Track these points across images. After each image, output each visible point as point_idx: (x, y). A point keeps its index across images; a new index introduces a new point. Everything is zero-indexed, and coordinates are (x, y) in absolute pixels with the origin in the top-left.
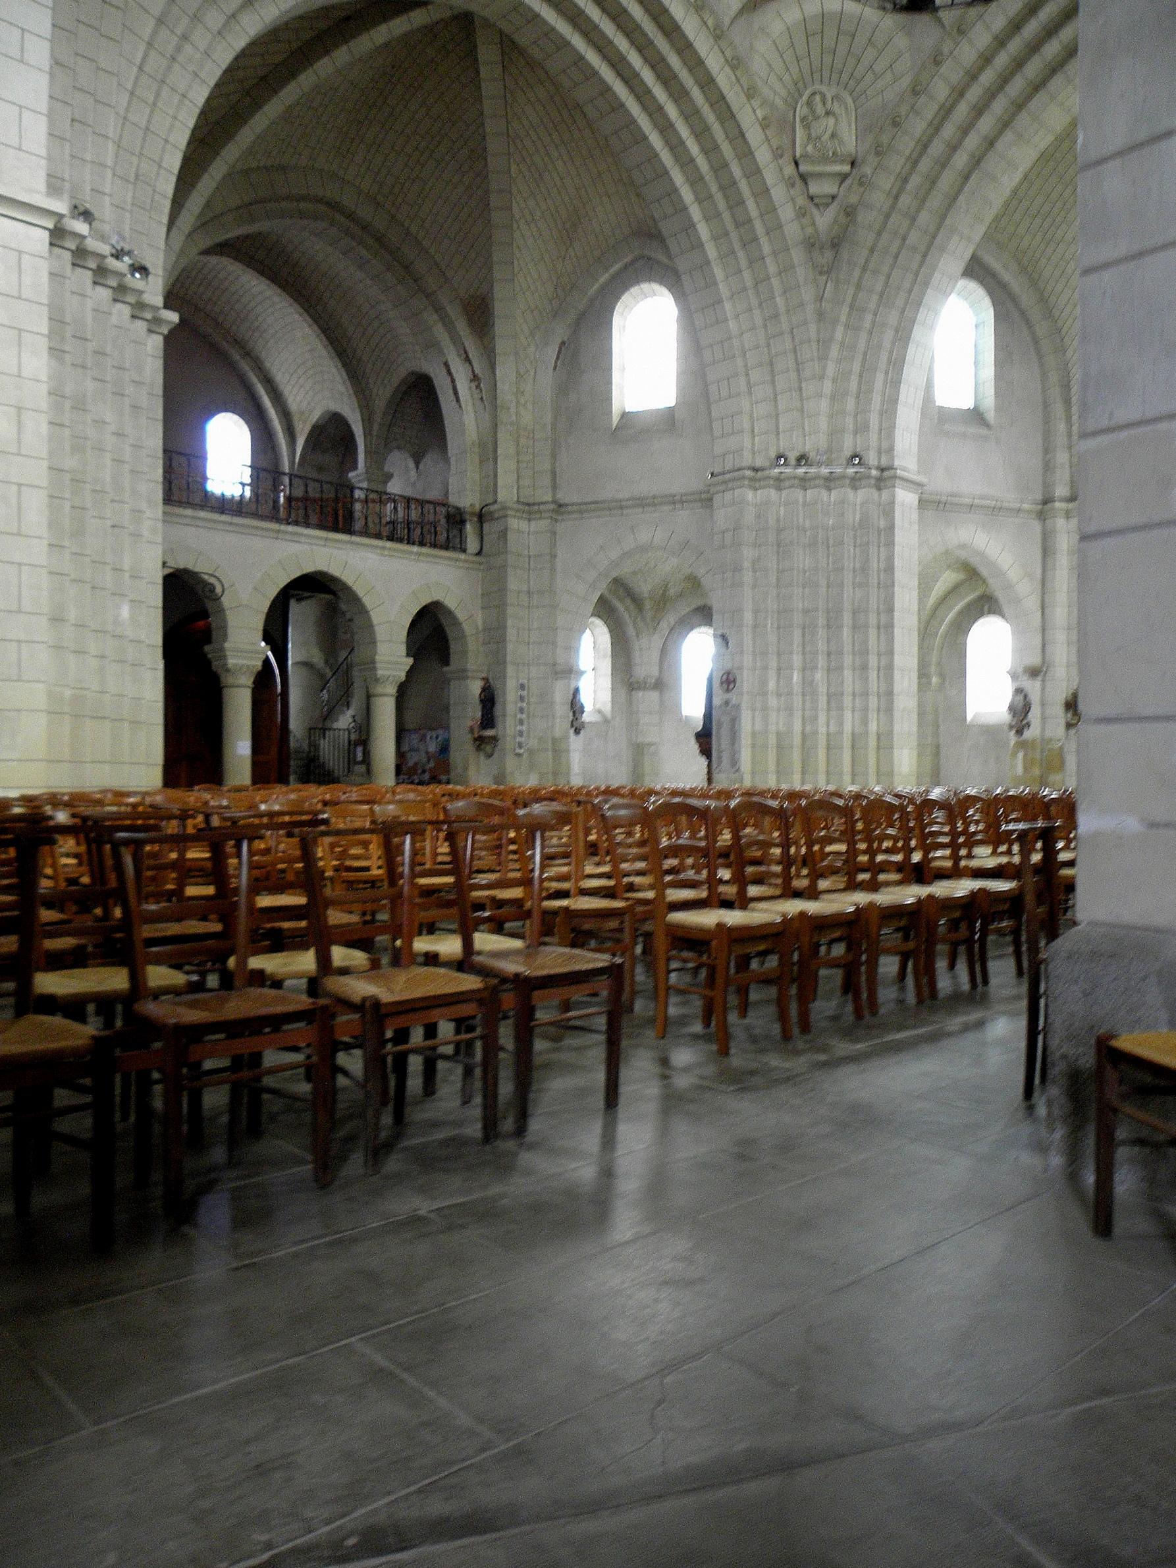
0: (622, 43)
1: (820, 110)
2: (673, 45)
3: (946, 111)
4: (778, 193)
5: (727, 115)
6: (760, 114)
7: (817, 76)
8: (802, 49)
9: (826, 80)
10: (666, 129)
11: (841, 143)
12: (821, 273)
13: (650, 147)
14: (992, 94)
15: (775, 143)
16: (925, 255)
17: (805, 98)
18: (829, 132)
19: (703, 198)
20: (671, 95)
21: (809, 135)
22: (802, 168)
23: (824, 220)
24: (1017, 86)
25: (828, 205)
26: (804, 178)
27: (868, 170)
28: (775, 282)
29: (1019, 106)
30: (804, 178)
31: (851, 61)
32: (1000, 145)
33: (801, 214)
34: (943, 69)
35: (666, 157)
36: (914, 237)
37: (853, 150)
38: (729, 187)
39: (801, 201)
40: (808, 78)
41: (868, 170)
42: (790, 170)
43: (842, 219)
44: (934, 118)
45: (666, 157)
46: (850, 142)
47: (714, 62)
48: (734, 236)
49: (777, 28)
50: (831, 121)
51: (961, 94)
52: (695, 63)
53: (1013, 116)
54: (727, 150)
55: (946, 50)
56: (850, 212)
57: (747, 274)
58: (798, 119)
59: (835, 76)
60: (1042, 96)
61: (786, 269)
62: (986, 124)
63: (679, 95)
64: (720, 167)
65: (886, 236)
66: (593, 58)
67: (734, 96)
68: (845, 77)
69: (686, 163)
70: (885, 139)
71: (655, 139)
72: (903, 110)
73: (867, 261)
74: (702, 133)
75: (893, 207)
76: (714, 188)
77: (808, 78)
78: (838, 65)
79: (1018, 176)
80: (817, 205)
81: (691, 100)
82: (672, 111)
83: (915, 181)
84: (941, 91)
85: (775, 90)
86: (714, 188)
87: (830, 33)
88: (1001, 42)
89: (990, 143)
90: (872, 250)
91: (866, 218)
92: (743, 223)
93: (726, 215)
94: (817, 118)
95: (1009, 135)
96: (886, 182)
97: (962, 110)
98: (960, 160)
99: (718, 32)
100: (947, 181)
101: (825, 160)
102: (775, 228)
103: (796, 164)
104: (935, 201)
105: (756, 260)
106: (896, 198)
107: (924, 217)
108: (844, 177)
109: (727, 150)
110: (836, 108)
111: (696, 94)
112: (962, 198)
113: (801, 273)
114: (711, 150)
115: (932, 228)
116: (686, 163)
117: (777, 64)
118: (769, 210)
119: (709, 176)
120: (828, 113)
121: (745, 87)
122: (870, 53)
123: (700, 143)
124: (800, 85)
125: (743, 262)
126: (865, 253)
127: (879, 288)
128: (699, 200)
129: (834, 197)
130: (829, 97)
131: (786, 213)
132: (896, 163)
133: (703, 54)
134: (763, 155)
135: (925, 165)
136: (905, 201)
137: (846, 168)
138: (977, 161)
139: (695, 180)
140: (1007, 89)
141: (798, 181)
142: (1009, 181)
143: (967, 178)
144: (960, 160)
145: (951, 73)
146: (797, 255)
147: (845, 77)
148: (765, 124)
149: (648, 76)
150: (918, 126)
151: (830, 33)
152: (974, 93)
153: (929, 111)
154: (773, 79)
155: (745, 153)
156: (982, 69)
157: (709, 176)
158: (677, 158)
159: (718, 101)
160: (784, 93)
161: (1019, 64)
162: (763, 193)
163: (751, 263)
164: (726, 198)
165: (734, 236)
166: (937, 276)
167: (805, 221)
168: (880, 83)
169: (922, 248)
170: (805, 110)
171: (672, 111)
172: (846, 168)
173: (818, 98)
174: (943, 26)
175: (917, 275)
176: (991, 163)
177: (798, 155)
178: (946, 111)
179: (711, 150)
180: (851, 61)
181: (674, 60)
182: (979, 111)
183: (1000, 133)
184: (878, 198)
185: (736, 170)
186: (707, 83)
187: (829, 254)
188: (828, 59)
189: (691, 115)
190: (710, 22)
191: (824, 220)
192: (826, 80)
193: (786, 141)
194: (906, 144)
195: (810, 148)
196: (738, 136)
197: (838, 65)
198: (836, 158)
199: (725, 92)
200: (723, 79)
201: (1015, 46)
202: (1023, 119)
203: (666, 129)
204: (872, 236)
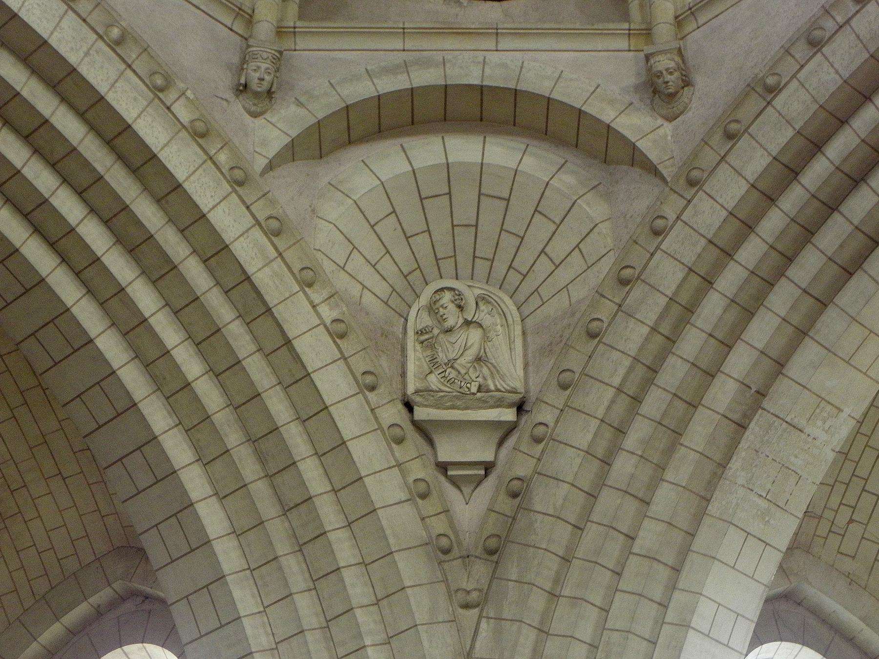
0: (120, 266)
1: (453, 318)
2: (146, 188)
3: (684, 310)
4: (368, 452)
5: (256, 309)
6: (328, 313)
7: (447, 266)
8: (413, 221)
9: (465, 271)
10: (133, 327)
11: (495, 371)
12: (466, 606)
13: (100, 357)
14: (766, 281)
15: (360, 364)
16: (677, 570)
17: (424, 299)
18: (470, 355)
19: (212, 456)
20: (144, 272)
21: (433, 361)
22: (421, 413)
23: (470, 511)
24: (809, 265)
25: (479, 481)
26: (421, 428)
27: (546, 415)
28: (365, 619)
29: (822, 302)
30: (421, 428)
31: (509, 243)
32: (796, 367)
33: (421, 493)
34: (669, 243)
35: (133, 379)
36: (649, 536)
37: (519, 385)
38: (264, 438)
39: (419, 471)
40: (429, 268)
41: (546, 415)
42: (393, 413)
43: (507, 505)
44: (661, 317)
45: (133, 379)
46: (511, 370)
47: (228, 219)
48: (277, 529)
49: (362, 183)
50: (475, 335)
51: (708, 282)
52: (192, 220)
53: (813, 319)
54: (258, 370)
55: (670, 213)
56: (518, 492)
57: (305, 604)
58: (411, 333)
59: (481, 266)
60: (859, 283)
61: (389, 596)
62: (762, 331)
63: (161, 272)
64: (246, 401)
65: (592, 532)
66: (88, 315)
67: (272, 281)
68: (500, 267)
69: (175, 390)
70: (574, 361)
71: (111, 347)
72: (605, 311)
73: (558, 580)
74: (207, 338)
75: (601, 482)
76: (233, 438)
77: (429, 268)
78: (485, 250)
79: (844, 428)
80: (455, 482)
81: (183, 281)
82: (145, 298)
83: (638, 432)
84: (668, 275)
85: (365, 284)
86: (233, 438)
87: (465, 196)
88: (767, 195)
89: (778, 365)
90: (566, 560)
91: (547, 498)
92: (294, 505)
93: (260, 490)
94: (449, 331)
95: (809, 352)
96: (581, 433)
97: (713, 307)
98: (723, 394)
99: (159, 81)
100: (701, 431)
101: (464, 400)
102: (362, 516)
103: (409, 406)
104: (683, 468)
105: (323, 576)
106: (607, 462)
107: (665, 498)
108: (508, 430)
109: (258, 370)
110: (484, 316)
111: (195, 273)
112: (735, 465)
113: (421, 603)
114: (226, 368)
115: (683, 521)
116: (175, 390)
117: (369, 246)
118: (349, 483)
119: (223, 418)
120: (468, 323)
121: (296, 268)
122: (541, 229)
123: (204, 356)
124: (416, 277)
125: (298, 580)
126: (553, 564)
127: (586, 632)
128: (204, 461)
129: (488, 467)
130: (470, 297)
131: (386, 489)
132: (598, 399)
133: (180, 174)
134: (333, 383)
135: (654, 403)
136: (624, 466)
137: (509, 415)
138: (757, 397)
139: (196, 423)
140: (791, 272)
141: (414, 438)
142: (828, 436)
143: (742, 427)
144: (723, 394)
145: (684, 247)
146: (411, 568)
147: (500, 267)
148: (338, 333)
149: (95, 236)
150: (633, 336)
151: (465, 196)
152: (731, 279)
153: (651, 308)
154: (356, 263)
155: (297, 377)
156: (739, 241)
157: (223, 418)
158: (158, 383)
159: (239, 285)
160: (382, 289)
161: (807, 231)
162: (334, 450)
163: (315, 580)
164: (262, 458)
165: (277, 529)
166: (705, 609)
167: (428, 507)
168: (563, 276)
169: (669, 558)
170: (426, 320)
171: (145, 298)
172: (509, 415)
173: (447, 296)
174: (652, 170)
175: (664, 606)
176: (783, 398)
177: (410, 389)
178: (684, 310)
179: (226, 368)
180: (509, 243)
181: (148, 213)
182: (747, 309)
183: (793, 346)
184: (568, 463)
185: (278, 407)
186: (216, 253)
187: (481, 570)
188: (465, 238)
189: (185, 307)
190: (222, 158)
191: (470, 511)
192: (465, 271)
193: (385, 365)
194: (614, 367)
195: (434, 381)
196: (281, 347)
197: (485, 250)
198: (485, 396)
199: (250, 270)
200: (249, 250)
201: (793, 200)
202: (831, 322)
203: (133, 327)
204: (563, 532)
